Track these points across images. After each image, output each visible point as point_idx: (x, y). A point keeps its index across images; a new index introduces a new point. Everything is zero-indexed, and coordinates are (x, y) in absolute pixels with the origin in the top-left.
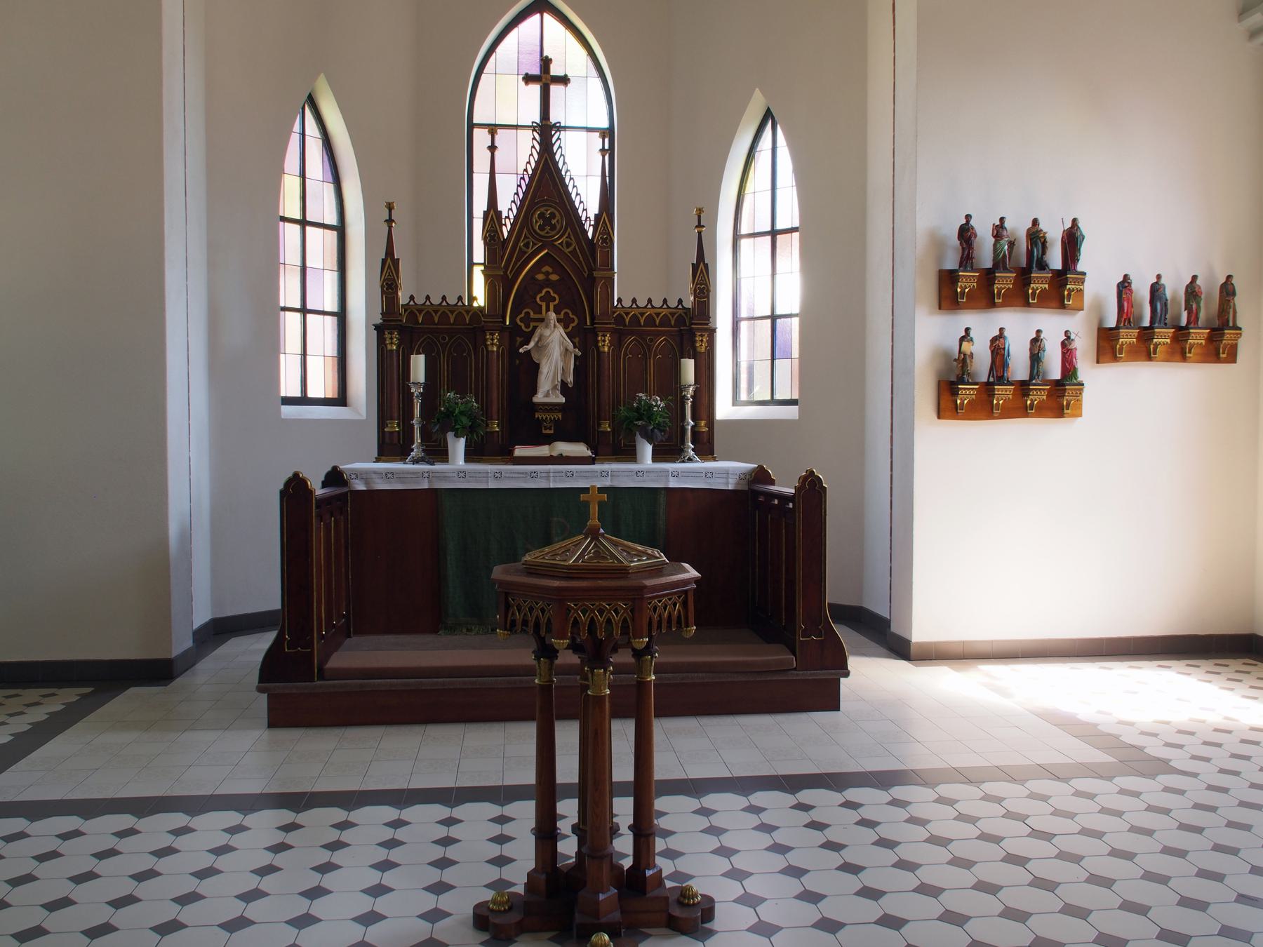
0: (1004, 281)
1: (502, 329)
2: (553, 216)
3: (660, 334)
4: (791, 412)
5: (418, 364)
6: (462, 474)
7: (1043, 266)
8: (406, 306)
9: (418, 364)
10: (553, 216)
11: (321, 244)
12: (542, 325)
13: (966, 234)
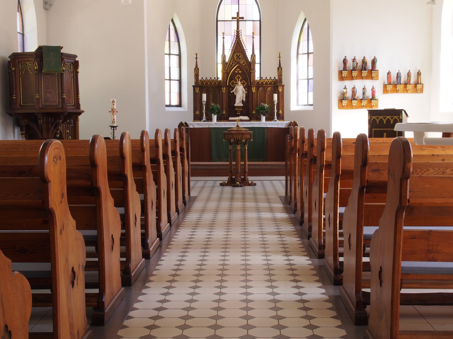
1: (226, 86)
2: (240, 55)
3: (269, 87)
4: (311, 108)
5: (204, 96)
6: (216, 124)
8: (201, 80)
9: (204, 96)
10: (240, 55)
12: (237, 85)
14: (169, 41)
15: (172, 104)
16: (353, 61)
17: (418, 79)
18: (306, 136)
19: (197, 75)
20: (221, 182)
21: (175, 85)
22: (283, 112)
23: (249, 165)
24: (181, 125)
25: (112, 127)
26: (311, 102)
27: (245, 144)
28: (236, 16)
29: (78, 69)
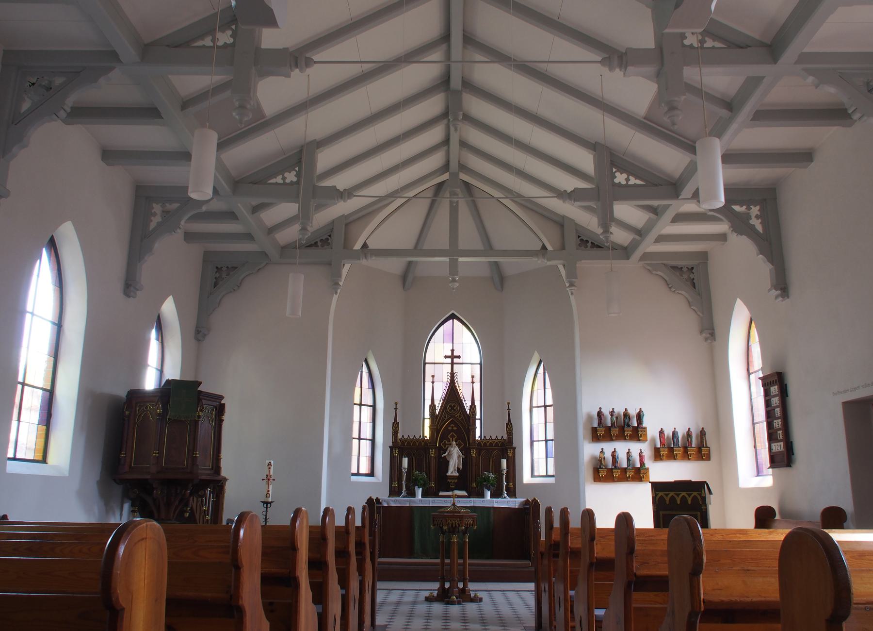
0: (615, 431)
1: (436, 448)
5: (405, 461)
6: (421, 501)
7: (629, 426)
9: (405, 461)
11: (367, 412)
13: (600, 414)
14: (361, 387)
15: (361, 472)
16: (612, 415)
17: (702, 442)
18: (557, 524)
19: (395, 432)
20: (427, 594)
21: (366, 446)
22: (514, 485)
23: (470, 565)
24: (370, 501)
25: (264, 503)
26: (551, 472)
27: (464, 533)
28: (450, 354)
29: (223, 415)
